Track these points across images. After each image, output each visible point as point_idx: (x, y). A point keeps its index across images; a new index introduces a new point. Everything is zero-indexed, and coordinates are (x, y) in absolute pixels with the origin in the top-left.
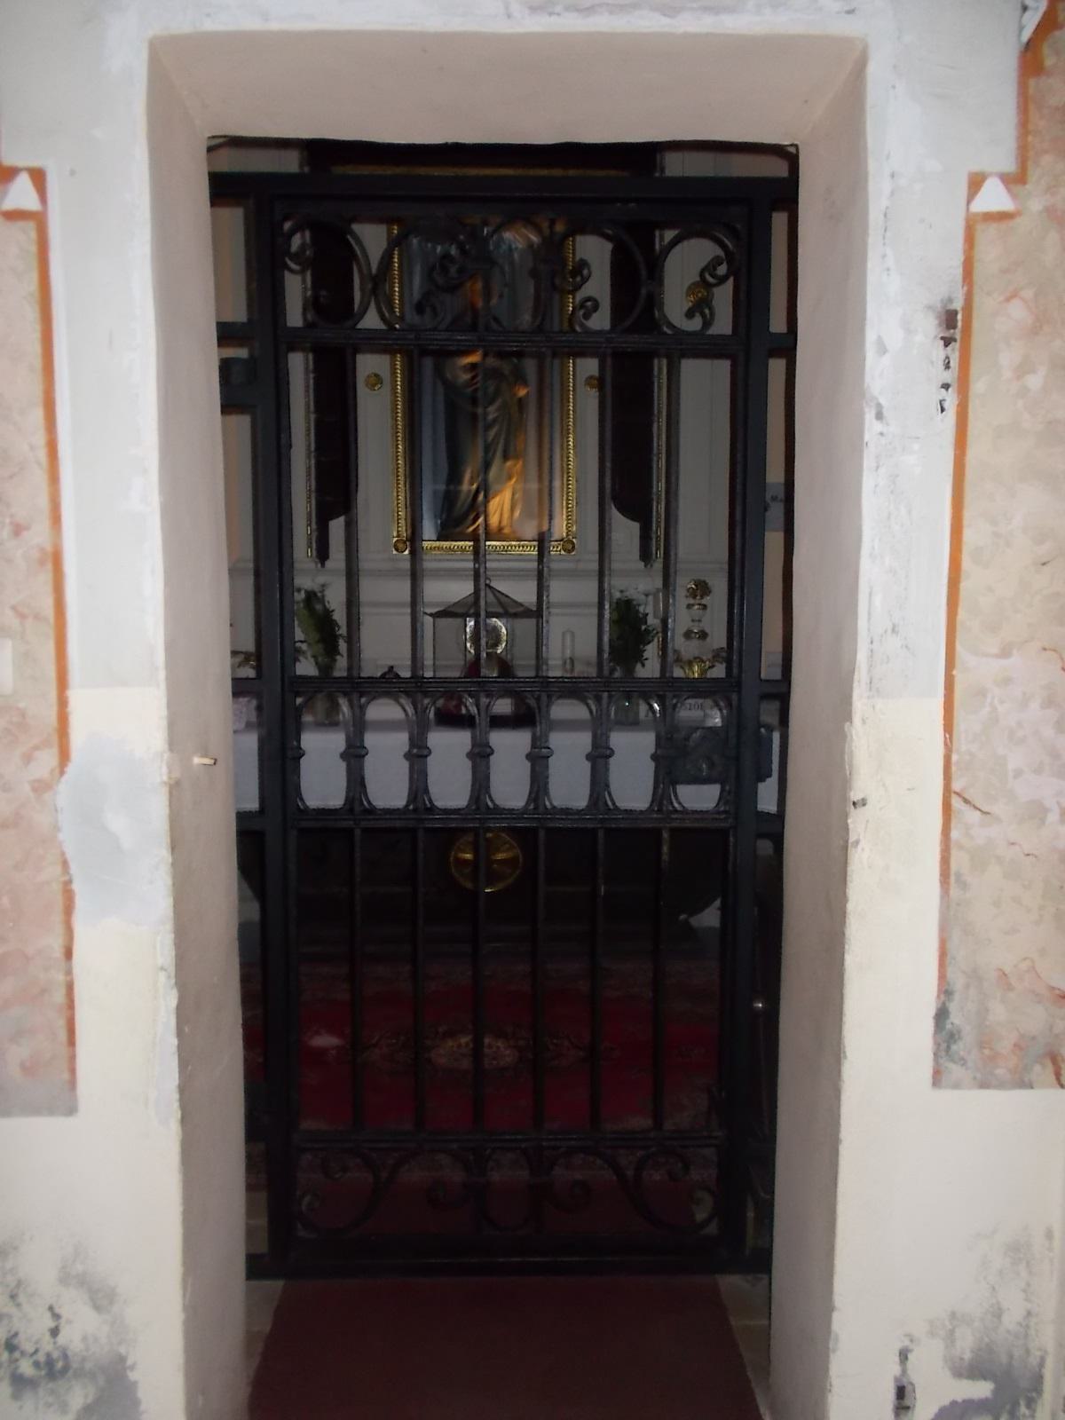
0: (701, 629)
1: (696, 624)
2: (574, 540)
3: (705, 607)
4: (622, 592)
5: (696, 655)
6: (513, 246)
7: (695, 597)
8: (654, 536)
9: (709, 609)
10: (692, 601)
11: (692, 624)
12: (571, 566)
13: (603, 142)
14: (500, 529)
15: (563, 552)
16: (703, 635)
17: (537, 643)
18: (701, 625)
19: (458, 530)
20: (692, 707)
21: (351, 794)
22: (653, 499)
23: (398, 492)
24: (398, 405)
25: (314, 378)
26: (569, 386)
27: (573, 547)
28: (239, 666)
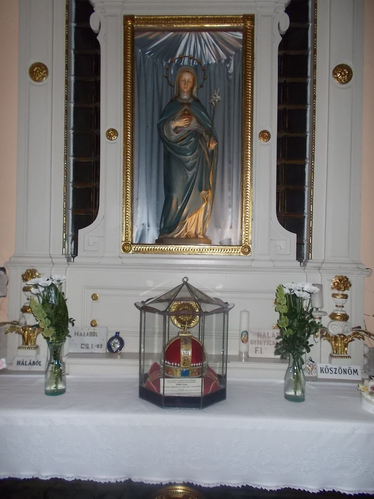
0: (343, 313)
1: (339, 309)
2: (250, 245)
3: (345, 297)
4: (290, 290)
5: (341, 333)
6: (210, 62)
7: (339, 289)
8: (305, 243)
9: (349, 299)
10: (336, 292)
11: (336, 308)
12: (248, 263)
13: (101, 59)
14: (196, 236)
15: (241, 254)
16: (345, 318)
17: (139, 101)
18: (343, 309)
19: (170, 235)
20: (337, 371)
21: (97, 183)
22: (304, 217)
23: (126, 210)
24: (127, 95)
25: (74, 134)
26: (248, 138)
27: (249, 251)
28: (6, 273)
